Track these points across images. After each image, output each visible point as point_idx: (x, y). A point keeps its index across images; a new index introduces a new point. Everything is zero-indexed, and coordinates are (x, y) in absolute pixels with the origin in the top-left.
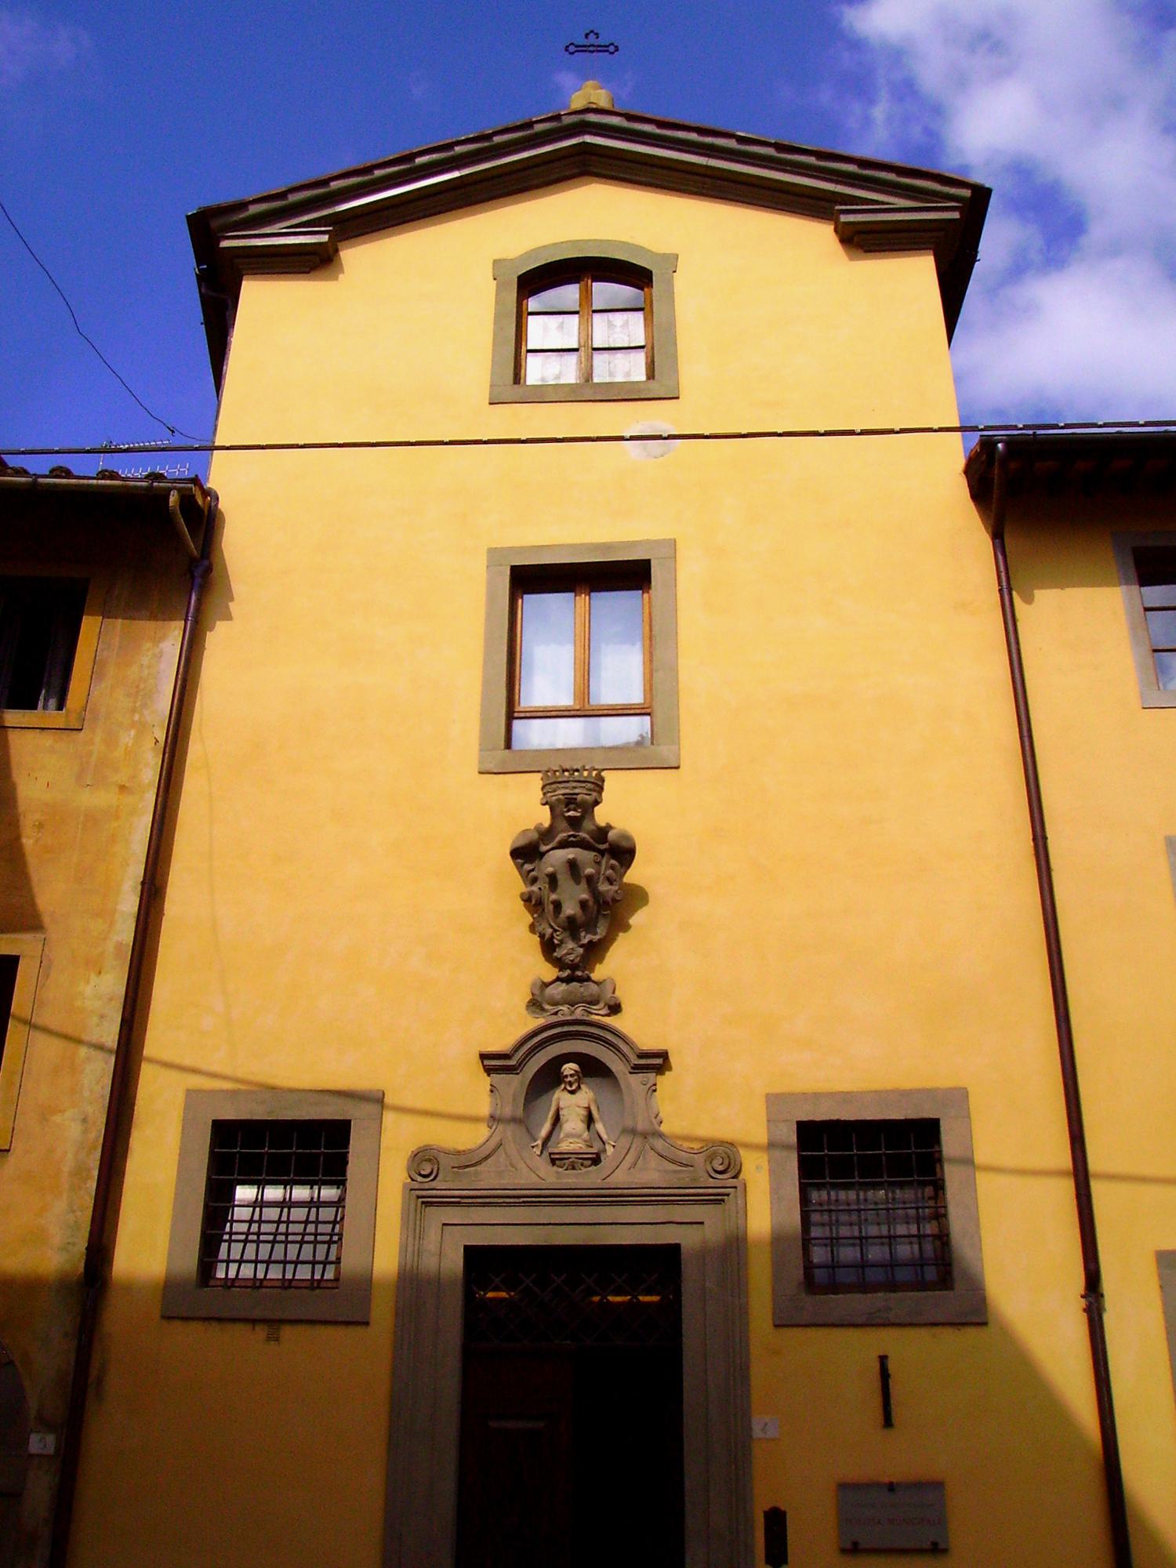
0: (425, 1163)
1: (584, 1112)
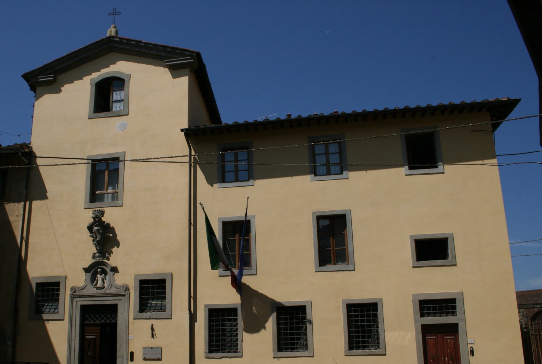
0: (74, 290)
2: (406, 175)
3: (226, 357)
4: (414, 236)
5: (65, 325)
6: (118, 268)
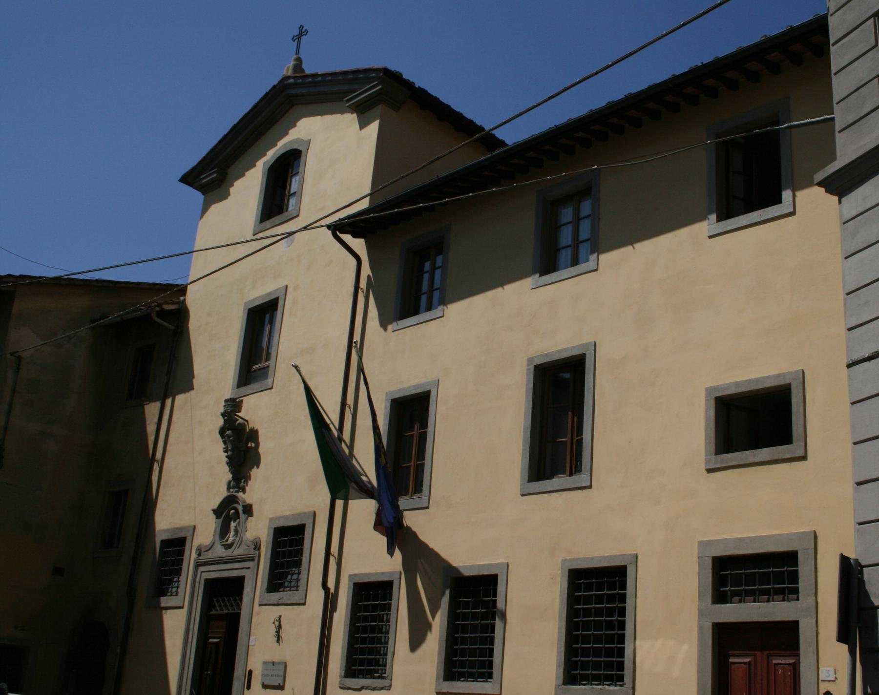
2: (710, 237)
3: (367, 688)
4: (716, 389)
5: (182, 614)
6: (254, 507)
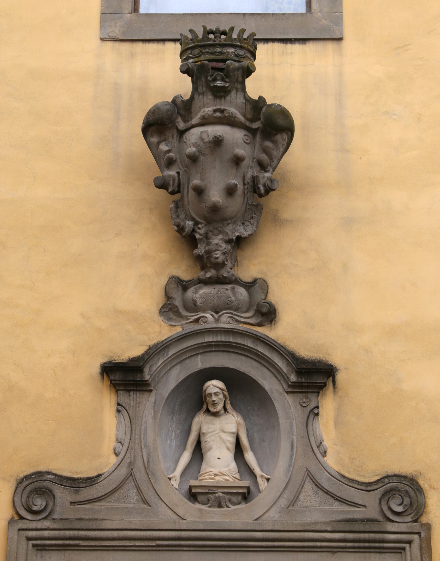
1: (232, 440)
